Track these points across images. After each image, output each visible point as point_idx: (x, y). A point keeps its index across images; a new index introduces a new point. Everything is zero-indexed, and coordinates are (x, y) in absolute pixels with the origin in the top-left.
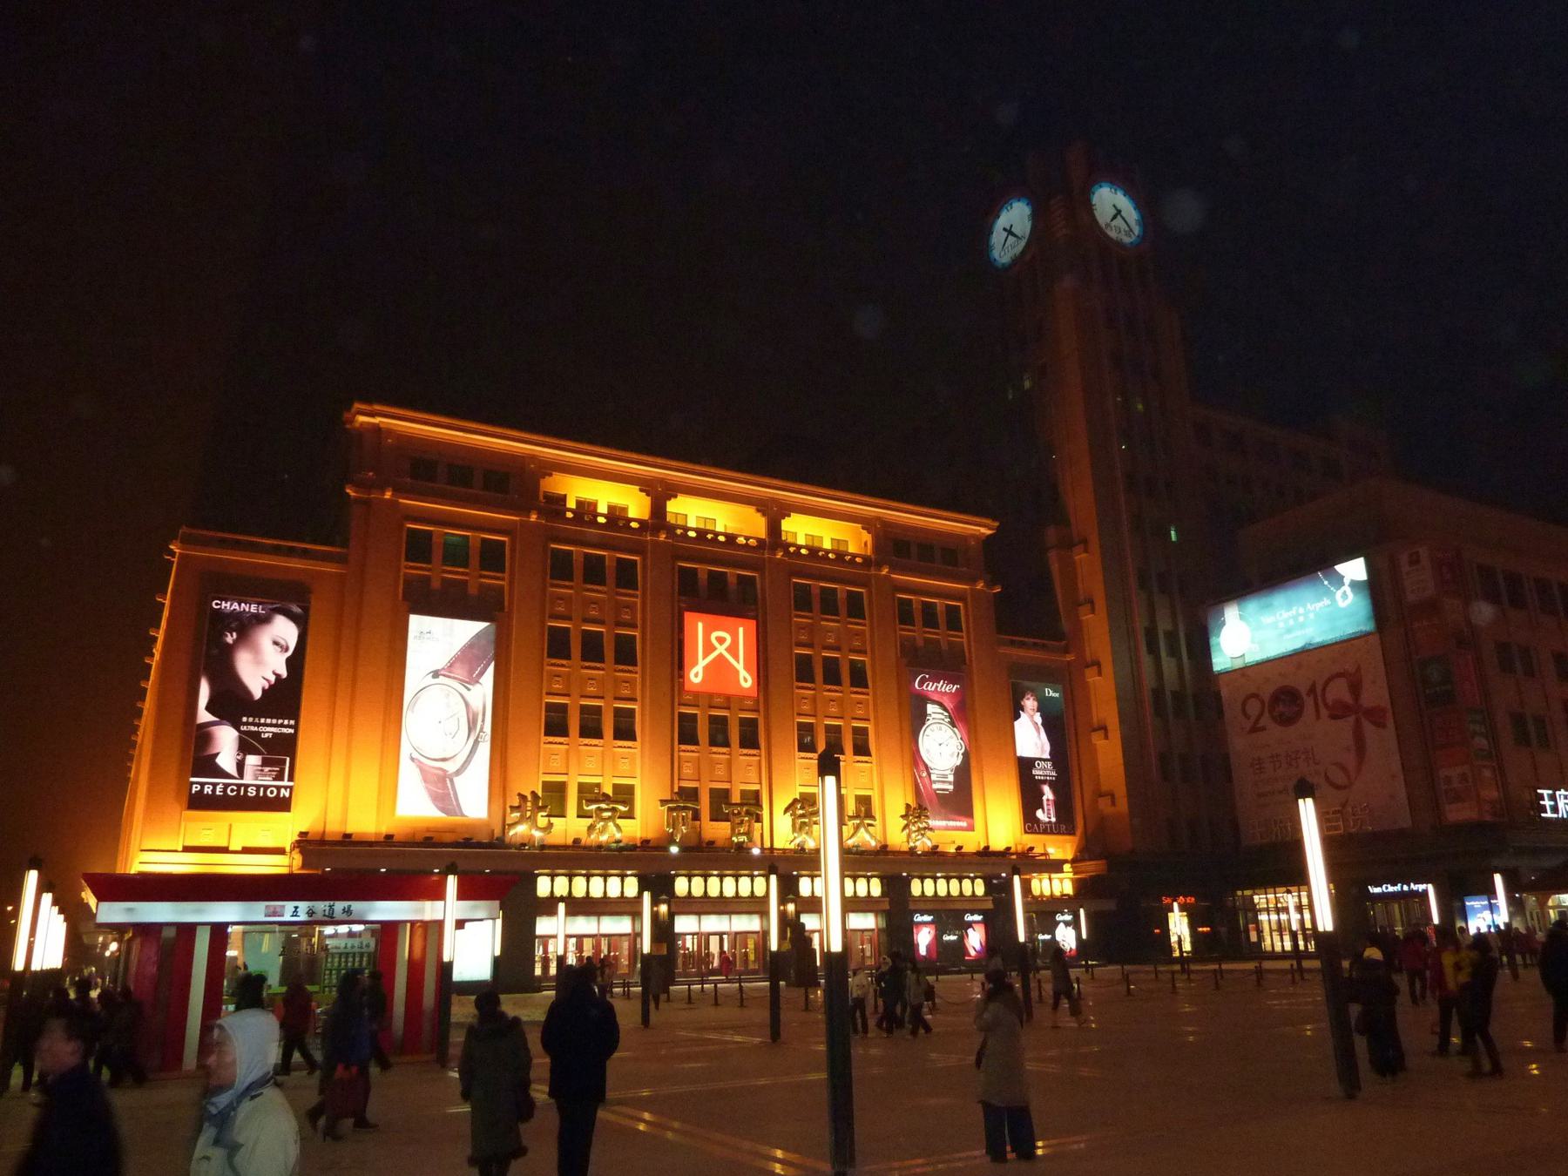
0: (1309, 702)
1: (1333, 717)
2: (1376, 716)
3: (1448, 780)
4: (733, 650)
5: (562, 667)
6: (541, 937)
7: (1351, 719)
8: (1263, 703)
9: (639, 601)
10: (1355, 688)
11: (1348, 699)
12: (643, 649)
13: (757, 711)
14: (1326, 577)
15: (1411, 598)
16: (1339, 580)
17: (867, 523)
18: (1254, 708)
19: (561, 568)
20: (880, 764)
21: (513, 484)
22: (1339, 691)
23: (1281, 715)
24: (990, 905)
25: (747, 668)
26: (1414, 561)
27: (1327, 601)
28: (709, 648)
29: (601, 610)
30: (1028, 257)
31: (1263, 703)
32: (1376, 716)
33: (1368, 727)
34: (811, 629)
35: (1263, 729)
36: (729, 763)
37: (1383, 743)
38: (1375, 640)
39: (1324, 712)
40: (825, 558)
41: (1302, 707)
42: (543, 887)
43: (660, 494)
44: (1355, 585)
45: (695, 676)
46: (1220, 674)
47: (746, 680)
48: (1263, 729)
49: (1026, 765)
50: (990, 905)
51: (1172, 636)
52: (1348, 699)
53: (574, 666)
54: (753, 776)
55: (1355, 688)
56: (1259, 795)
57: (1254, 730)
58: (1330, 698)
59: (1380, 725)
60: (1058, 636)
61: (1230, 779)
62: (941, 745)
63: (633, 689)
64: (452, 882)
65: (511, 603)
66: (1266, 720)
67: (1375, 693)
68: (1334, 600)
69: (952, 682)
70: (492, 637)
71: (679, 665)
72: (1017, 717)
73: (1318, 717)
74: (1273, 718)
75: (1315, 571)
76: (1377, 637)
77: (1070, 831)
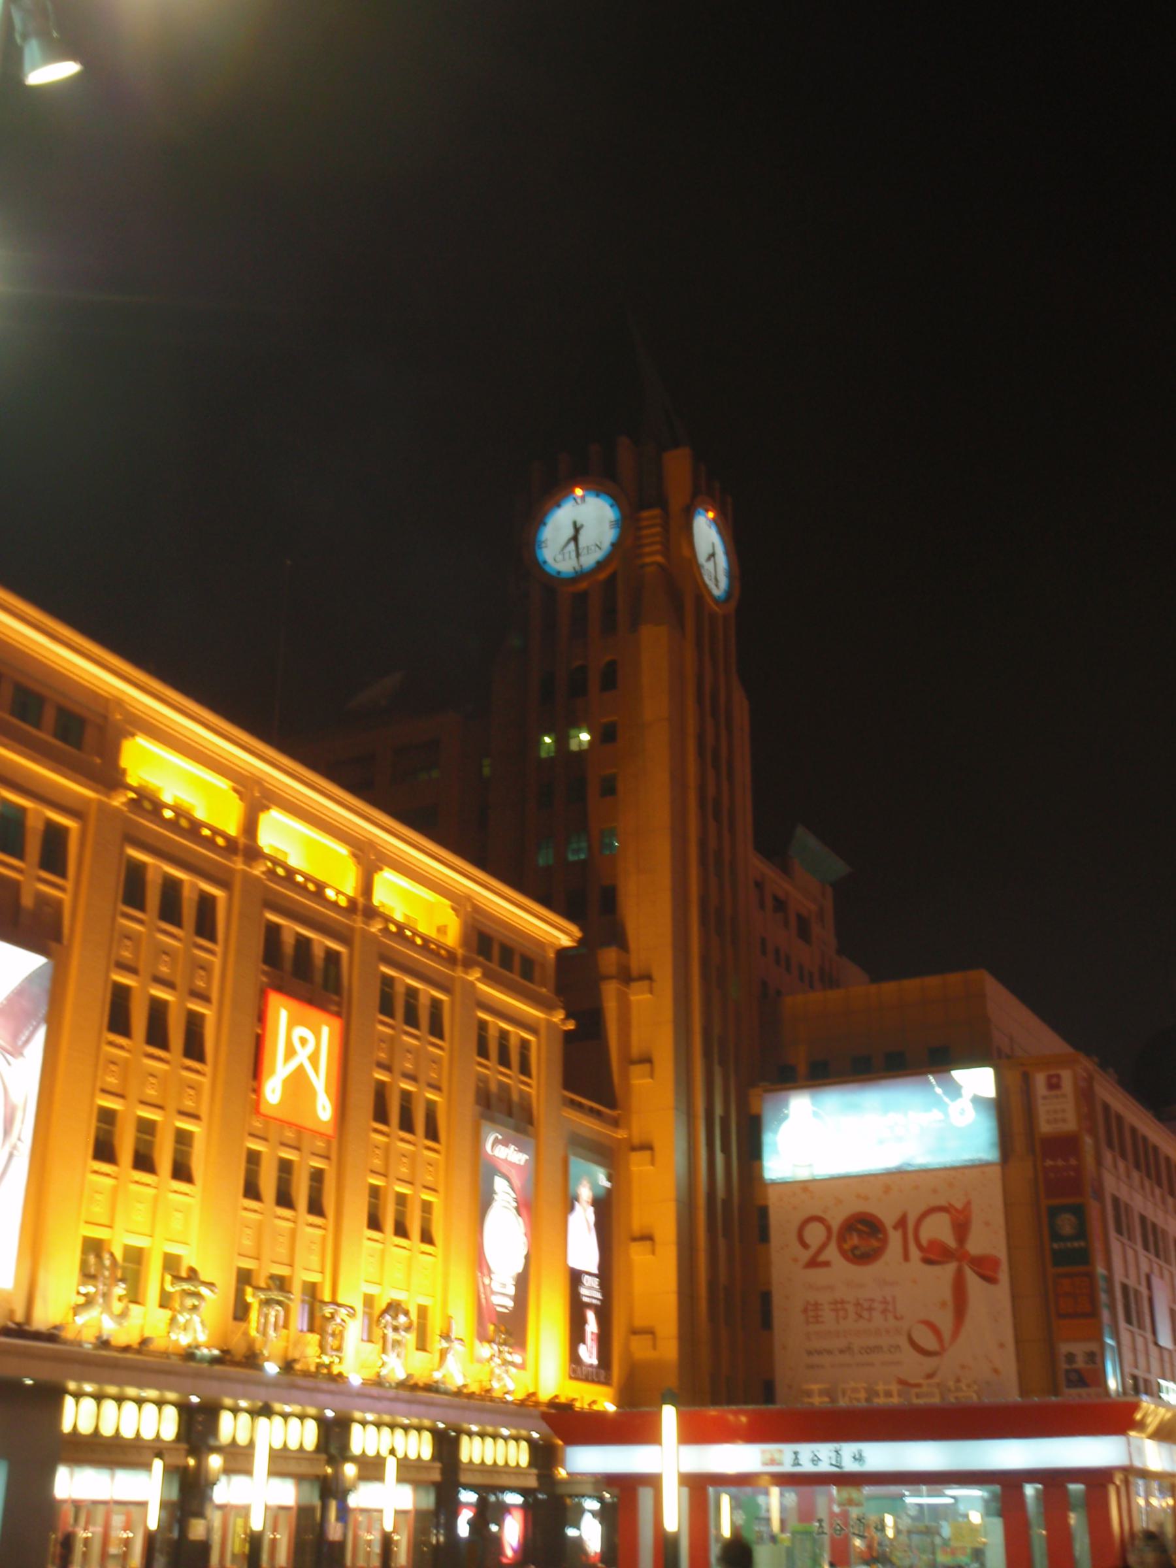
0: (895, 1237)
1: (927, 1261)
2: (985, 1268)
3: (1071, 1357)
4: (314, 1059)
5: (119, 1049)
6: (221, 1507)
7: (950, 1268)
8: (829, 1229)
9: (216, 961)
10: (961, 1228)
11: (951, 1242)
12: (539, 1058)
13: (327, 1158)
14: (939, 1084)
15: (1045, 1128)
16: (955, 1090)
17: (459, 901)
18: (815, 1234)
19: (133, 887)
20: (446, 1261)
21: (83, 735)
22: (939, 1229)
23: (855, 1248)
24: (532, 1482)
25: (327, 1092)
26: (1054, 1084)
27: (936, 1114)
28: (290, 1052)
29: (136, 952)
30: (602, 576)
31: (829, 1229)
32: (985, 1268)
33: (973, 1281)
34: (392, 1041)
35: (826, 1264)
36: (293, 1234)
37: (991, 1304)
38: (996, 1172)
39: (915, 1253)
40: (410, 942)
41: (885, 1242)
42: (78, 1415)
43: (257, 799)
44: (977, 1100)
45: (273, 1091)
46: (774, 1183)
47: (324, 1110)
48: (826, 1264)
49: (576, 1277)
50: (532, 1482)
51: (725, 1121)
52: (951, 1242)
53: (131, 1049)
54: (315, 1260)
55: (961, 1228)
56: (810, 1353)
57: (813, 1263)
58: (926, 1235)
59: (991, 1280)
60: (612, 1103)
61: (766, 1321)
62: (506, 1235)
63: (198, 1101)
64: (669, 1415)
65: (72, 930)
66: (832, 1253)
67: (988, 1238)
68: (946, 1114)
69: (521, 1149)
70: (46, 983)
71: (257, 1071)
72: (572, 1208)
73: (906, 1257)
74: (843, 1253)
75: (925, 1073)
76: (998, 1169)
77: (607, 1382)
